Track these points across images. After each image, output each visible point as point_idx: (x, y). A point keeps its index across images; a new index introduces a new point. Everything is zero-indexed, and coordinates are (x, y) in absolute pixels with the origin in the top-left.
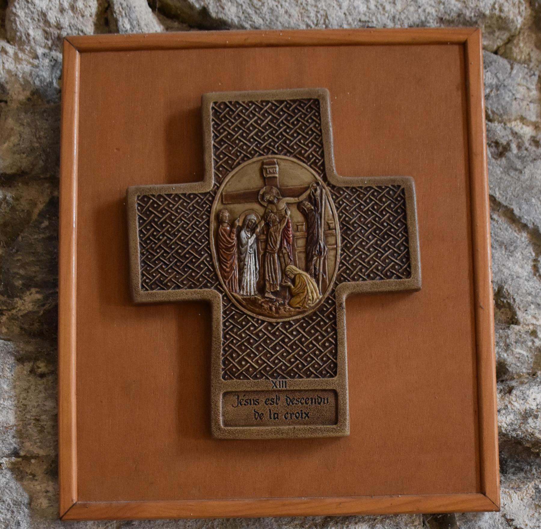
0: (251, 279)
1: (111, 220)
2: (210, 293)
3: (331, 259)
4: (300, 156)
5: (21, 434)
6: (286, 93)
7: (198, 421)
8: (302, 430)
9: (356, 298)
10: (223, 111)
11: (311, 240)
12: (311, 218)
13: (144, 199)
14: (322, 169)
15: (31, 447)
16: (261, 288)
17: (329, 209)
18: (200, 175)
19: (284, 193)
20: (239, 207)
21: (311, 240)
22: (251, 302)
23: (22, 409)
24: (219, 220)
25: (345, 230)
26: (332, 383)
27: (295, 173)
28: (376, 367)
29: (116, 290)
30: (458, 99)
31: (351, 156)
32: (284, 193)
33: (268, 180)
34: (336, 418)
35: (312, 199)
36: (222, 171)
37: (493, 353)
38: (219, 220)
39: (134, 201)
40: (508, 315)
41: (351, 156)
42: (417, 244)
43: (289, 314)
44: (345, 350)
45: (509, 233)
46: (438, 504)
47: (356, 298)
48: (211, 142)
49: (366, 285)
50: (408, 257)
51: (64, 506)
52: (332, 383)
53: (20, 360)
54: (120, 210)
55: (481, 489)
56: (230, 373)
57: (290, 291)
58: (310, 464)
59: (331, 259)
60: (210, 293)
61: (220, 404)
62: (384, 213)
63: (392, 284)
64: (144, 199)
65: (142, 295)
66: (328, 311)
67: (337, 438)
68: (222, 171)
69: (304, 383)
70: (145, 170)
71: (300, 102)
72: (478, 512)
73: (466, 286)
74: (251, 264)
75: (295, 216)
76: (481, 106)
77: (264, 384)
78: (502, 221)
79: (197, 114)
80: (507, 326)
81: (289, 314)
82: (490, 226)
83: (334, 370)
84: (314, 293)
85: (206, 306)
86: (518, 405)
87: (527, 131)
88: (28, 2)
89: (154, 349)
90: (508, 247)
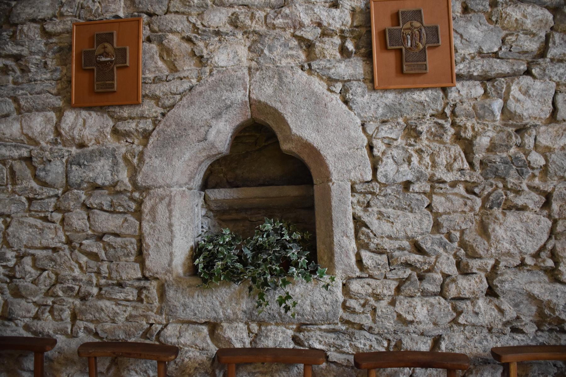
0: (409, 44)
1: (383, 34)
2: (402, 47)
3: (424, 40)
4: (417, 21)
5: (364, 75)
6: (414, 9)
7: (400, 71)
8: (420, 72)
9: (429, 47)
10: (403, 13)
11: (420, 37)
12: (420, 32)
13: (389, 30)
14: (422, 23)
15: (367, 77)
16: (411, 46)
17: (423, 31)
18: (399, 25)
19: (415, 28)
20: (407, 31)
21: (420, 37)
22: (410, 48)
23: (364, 70)
24: (403, 33)
25: (427, 35)
26: (425, 63)
27: (417, 24)
28: (433, 59)
29: (384, 47)
30: (446, 8)
31: (427, 20)
32: (415, 28)
33: (412, 26)
34: (426, 69)
35: (420, 29)
36: (404, 24)
37: (454, 58)
38: (403, 33)
39: (387, 30)
40: (456, 51)
41: (427, 20)
42: (440, 37)
43: (417, 50)
44: (427, 57)
45: (456, 35)
46: (444, 85)
47: (429, 47)
48: (401, 19)
49: (431, 45)
50: (438, 39)
51: (375, 87)
52: (425, 63)
53: (363, 61)
54: (384, 31)
55: (452, 82)
56: (406, 62)
57: (417, 46)
58: (421, 78)
59: (424, 40)
60: (402, 47)
61: (405, 67)
62: (434, 31)
63: (435, 45)
64: (389, 30)
65: (389, 47)
66: (424, 50)
67: (425, 73)
68: (404, 24)
69: (420, 63)
70: (387, 24)
71: (417, 11)
72: (452, 87)
73: (448, 44)
74: (409, 41)
75: (417, 32)
76: (451, 10)
77: (412, 63)
78: (455, 33)
79: (397, 14)
80: (523, 90)
81: (417, 50)
82: (453, 34)
83: (425, 60)
84: (421, 47)
85: (401, 50)
86: (458, 68)
87: (459, 15)
88: (564, 130)
89: (391, 57)
90: (456, 38)
